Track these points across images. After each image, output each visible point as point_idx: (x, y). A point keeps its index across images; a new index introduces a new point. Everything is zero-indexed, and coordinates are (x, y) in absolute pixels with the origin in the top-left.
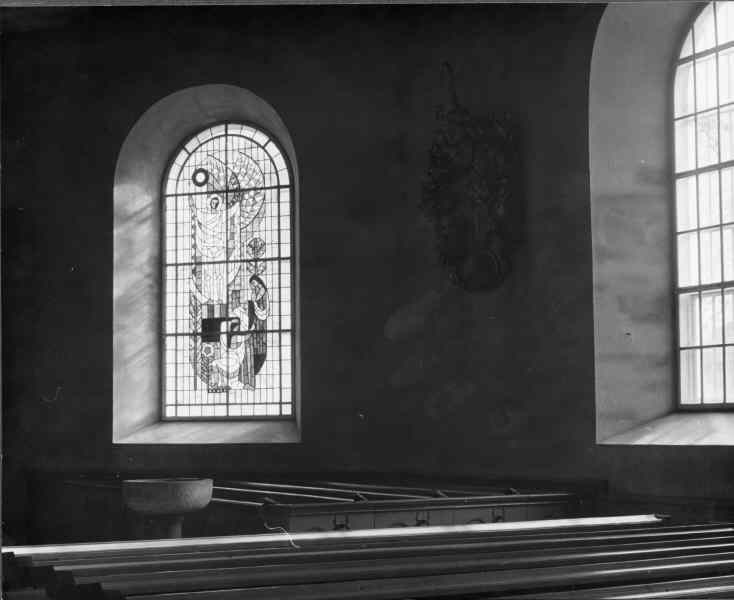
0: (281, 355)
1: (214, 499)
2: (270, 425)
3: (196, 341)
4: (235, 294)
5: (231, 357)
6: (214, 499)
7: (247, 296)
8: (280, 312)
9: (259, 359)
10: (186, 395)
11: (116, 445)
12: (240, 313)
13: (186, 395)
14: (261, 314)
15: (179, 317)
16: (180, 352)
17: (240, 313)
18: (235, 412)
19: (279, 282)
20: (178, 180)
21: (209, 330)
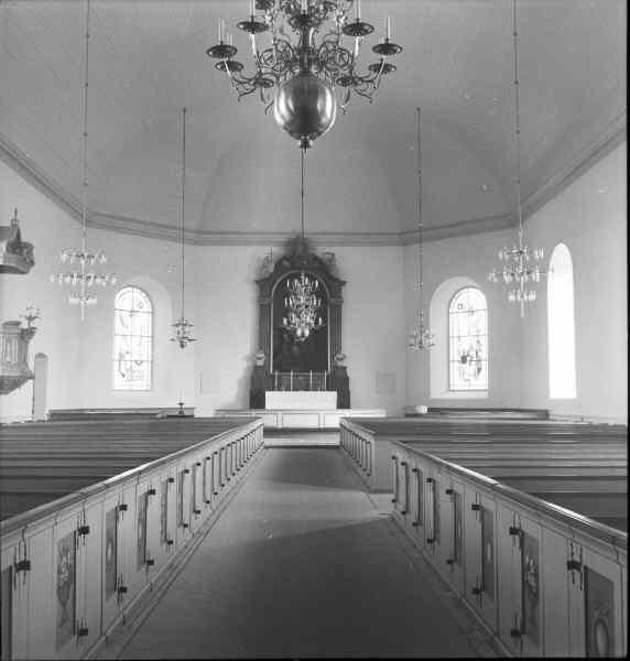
0: (485, 371)
1: (522, 305)
2: (275, 450)
3: (309, 86)
4: (471, 348)
5: (470, 368)
6: (522, 305)
7: (475, 347)
8: (484, 355)
9: (479, 370)
10: (458, 383)
11: (554, 400)
12: (473, 353)
13: (458, 383)
14: (480, 354)
15: (455, 356)
16: (455, 366)
17: (473, 353)
18: (472, 388)
19: (484, 341)
20: (454, 307)
21: (464, 360)
